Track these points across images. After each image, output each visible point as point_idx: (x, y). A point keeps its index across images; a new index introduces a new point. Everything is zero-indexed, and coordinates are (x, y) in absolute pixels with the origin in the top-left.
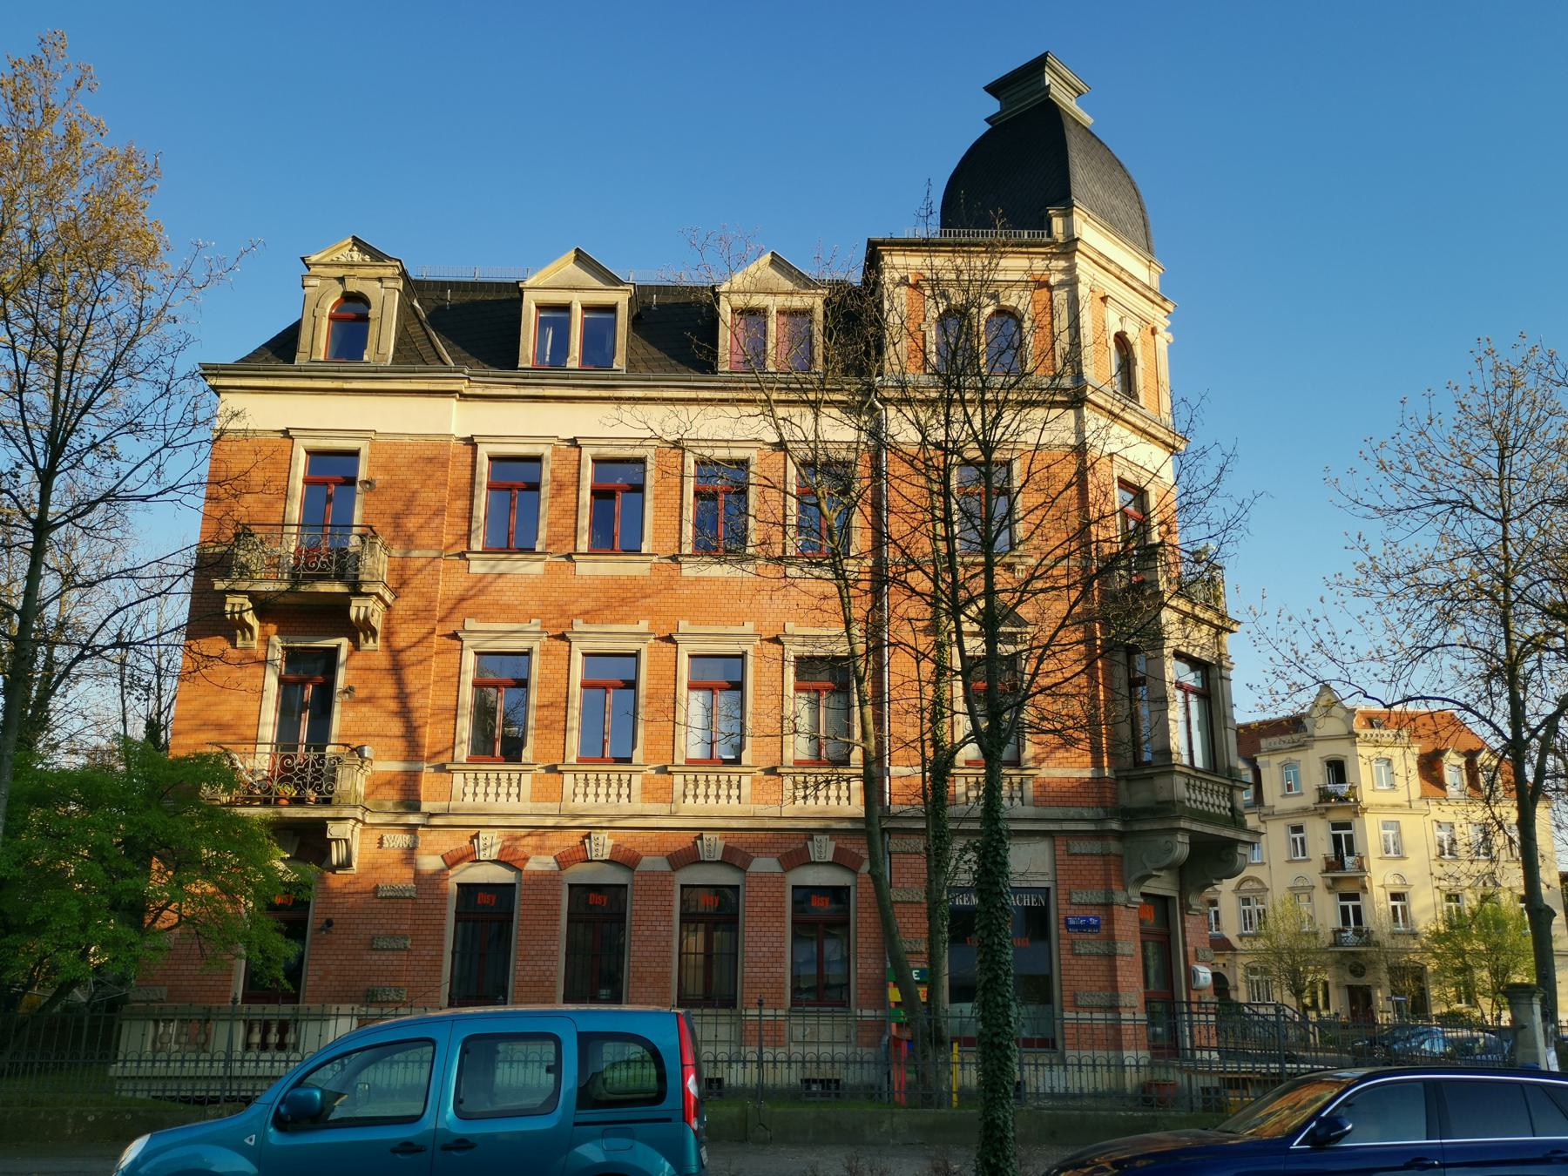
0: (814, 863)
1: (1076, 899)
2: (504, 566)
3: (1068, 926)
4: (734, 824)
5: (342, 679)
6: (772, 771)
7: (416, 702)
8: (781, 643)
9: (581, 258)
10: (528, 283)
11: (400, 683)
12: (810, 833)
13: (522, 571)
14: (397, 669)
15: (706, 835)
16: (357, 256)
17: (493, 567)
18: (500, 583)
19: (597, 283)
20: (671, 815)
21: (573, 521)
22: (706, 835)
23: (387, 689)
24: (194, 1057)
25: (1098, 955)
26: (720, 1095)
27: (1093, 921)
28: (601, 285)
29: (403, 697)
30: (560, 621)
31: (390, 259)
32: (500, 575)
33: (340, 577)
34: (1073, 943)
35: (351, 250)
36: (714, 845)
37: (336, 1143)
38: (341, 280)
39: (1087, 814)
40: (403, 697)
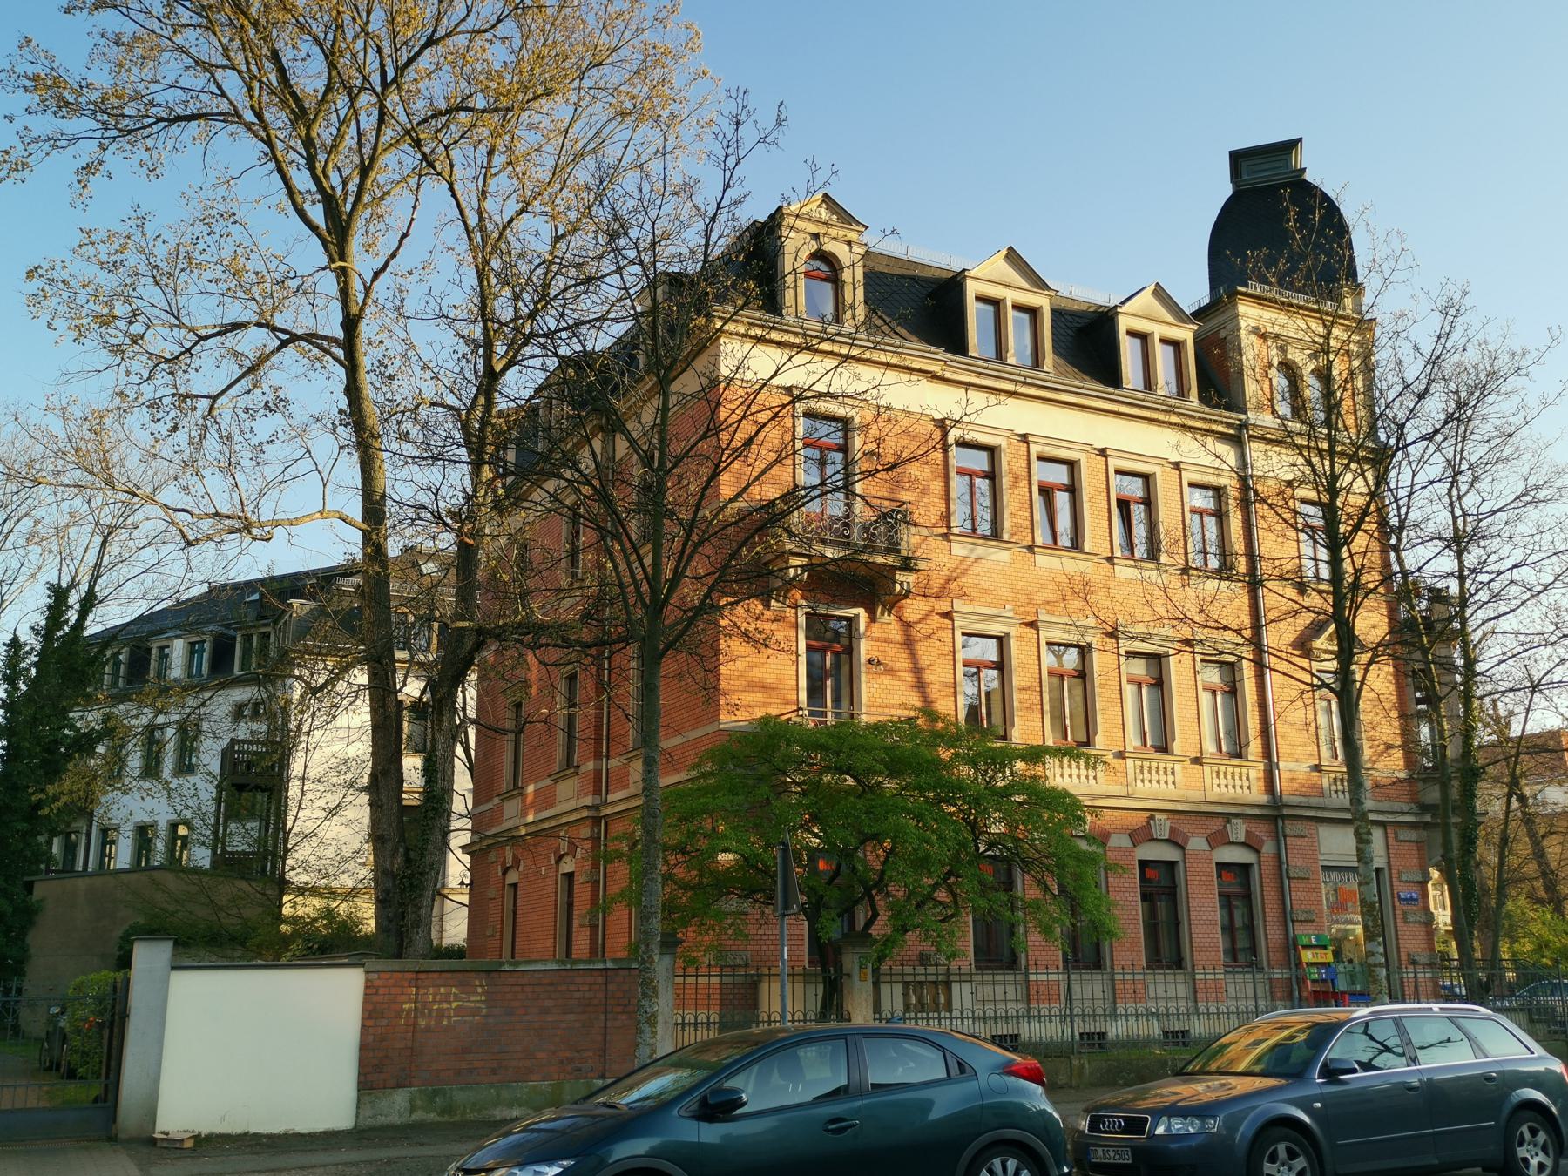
0: (1157, 840)
1: (1404, 878)
2: (980, 551)
3: (1400, 899)
4: (1180, 807)
5: (865, 649)
6: (1197, 761)
7: (928, 676)
8: (1117, 638)
9: (1013, 257)
10: (972, 273)
11: (913, 657)
12: (1227, 817)
13: (994, 557)
14: (909, 643)
15: (1158, 816)
16: (824, 214)
17: (972, 550)
18: (977, 567)
19: (1024, 284)
20: (1128, 797)
21: (1028, 514)
22: (1158, 816)
23: (903, 663)
24: (936, 1015)
25: (1420, 923)
26: (1184, 1044)
27: (1415, 896)
28: (1026, 286)
29: (917, 671)
30: (1028, 609)
31: (858, 223)
32: (977, 559)
33: (888, 551)
34: (1405, 913)
35: (819, 206)
36: (1163, 827)
37: (1470, 1077)
38: (816, 236)
39: (1406, 808)
40: (917, 671)
